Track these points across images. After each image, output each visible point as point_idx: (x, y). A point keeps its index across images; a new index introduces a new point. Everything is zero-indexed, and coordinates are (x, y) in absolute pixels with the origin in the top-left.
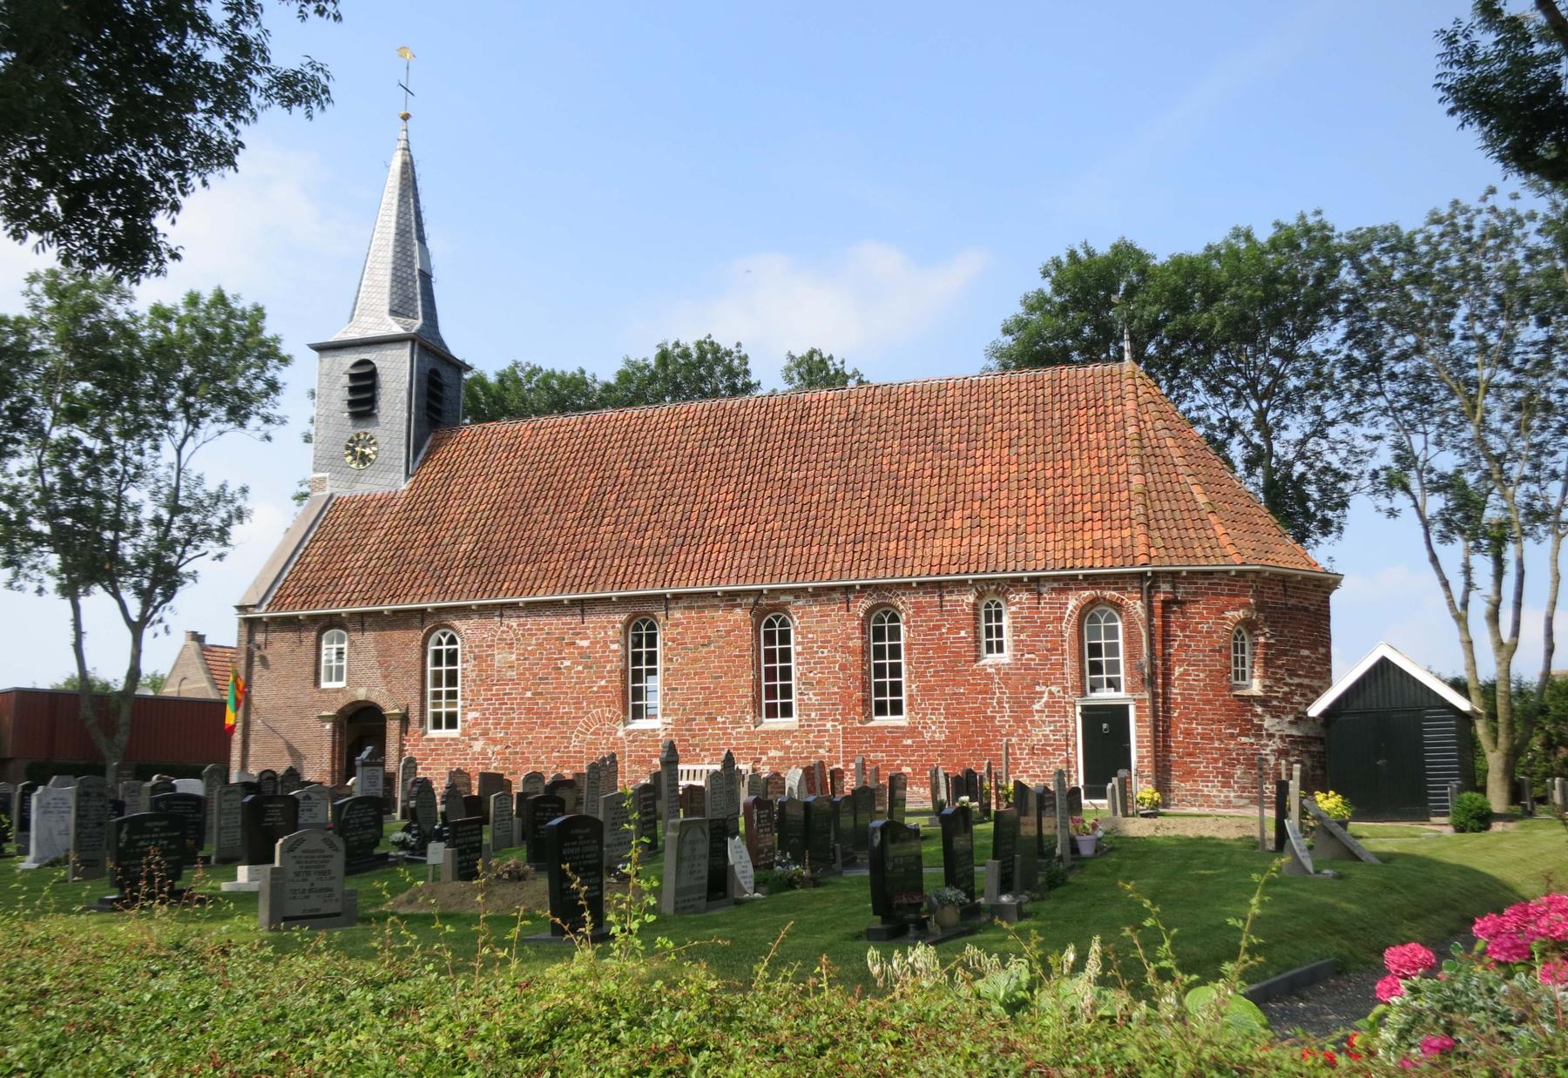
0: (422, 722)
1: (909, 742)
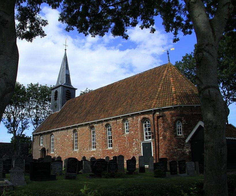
0: (50, 151)
1: (112, 153)
